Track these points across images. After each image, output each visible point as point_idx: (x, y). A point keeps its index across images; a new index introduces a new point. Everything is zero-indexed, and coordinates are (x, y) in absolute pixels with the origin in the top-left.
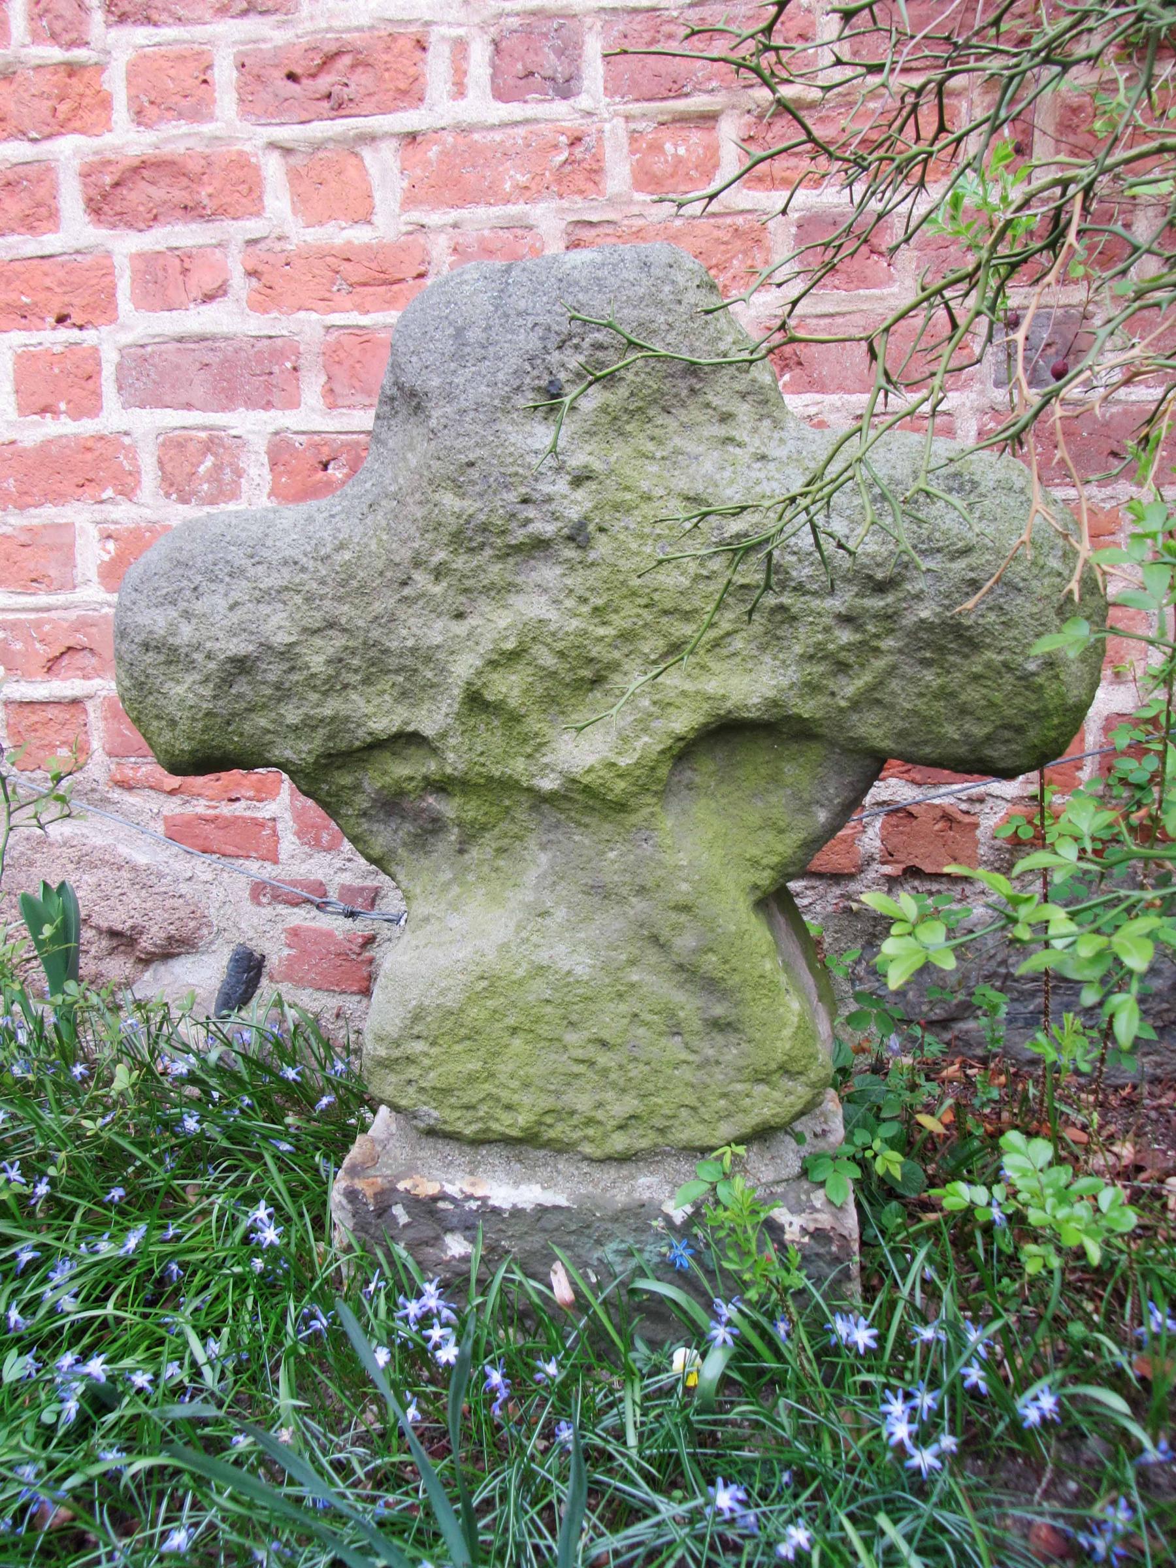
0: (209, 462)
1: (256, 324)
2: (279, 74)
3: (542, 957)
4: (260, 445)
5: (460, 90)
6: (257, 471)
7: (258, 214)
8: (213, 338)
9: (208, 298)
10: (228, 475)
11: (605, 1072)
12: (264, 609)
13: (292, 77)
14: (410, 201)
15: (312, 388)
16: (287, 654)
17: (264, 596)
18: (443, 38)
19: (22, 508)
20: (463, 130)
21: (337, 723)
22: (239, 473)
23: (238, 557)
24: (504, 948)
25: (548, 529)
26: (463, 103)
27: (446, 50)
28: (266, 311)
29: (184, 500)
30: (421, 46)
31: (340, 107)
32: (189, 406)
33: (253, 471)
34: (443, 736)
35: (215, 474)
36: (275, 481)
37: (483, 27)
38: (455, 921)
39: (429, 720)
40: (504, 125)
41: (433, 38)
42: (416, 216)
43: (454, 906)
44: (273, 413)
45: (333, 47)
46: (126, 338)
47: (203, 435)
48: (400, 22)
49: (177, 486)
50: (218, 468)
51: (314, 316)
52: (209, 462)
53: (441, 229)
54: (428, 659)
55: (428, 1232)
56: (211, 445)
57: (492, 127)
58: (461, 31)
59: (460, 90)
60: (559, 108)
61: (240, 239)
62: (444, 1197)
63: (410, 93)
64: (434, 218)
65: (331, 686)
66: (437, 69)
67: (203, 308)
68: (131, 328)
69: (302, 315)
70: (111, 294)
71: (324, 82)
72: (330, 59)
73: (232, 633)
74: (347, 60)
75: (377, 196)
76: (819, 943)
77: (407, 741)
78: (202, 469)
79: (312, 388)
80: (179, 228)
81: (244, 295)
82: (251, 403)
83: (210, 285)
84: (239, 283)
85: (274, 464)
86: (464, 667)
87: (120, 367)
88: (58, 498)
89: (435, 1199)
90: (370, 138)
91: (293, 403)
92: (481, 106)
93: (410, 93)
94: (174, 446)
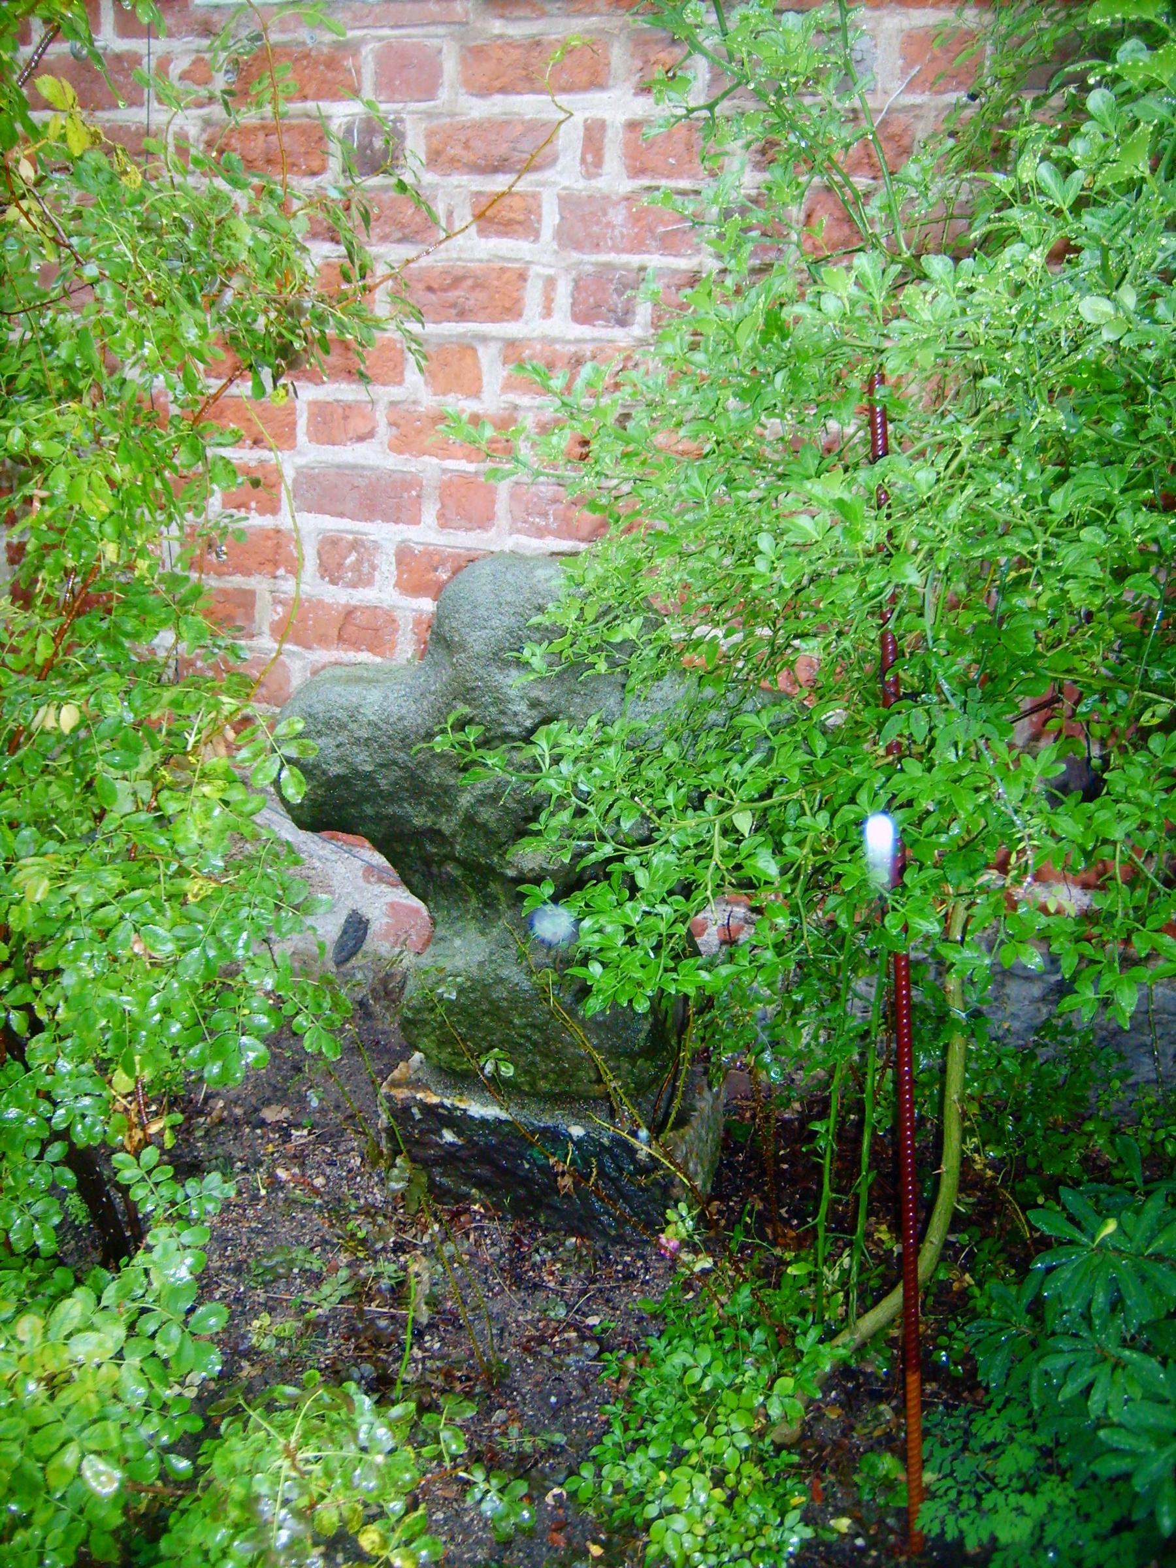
0: (353, 557)
1: (392, 462)
2: (421, 286)
3: (504, 973)
4: (390, 549)
5: (548, 312)
6: (387, 566)
7: (400, 383)
8: (363, 467)
9: (361, 439)
10: (366, 568)
11: (535, 1044)
12: (356, 749)
13: (430, 289)
14: (508, 386)
15: (430, 512)
16: (368, 777)
17: (357, 742)
18: (538, 275)
19: (220, 575)
20: (548, 341)
21: (395, 819)
22: (374, 568)
23: (342, 715)
24: (481, 964)
25: (515, 730)
26: (549, 322)
27: (540, 284)
28: (401, 453)
29: (333, 582)
30: (522, 277)
31: (463, 315)
32: (341, 515)
33: (384, 567)
34: (454, 836)
35: (357, 567)
36: (400, 576)
37: (567, 270)
38: (458, 942)
39: (448, 824)
40: (578, 341)
41: (531, 273)
42: (511, 397)
43: (458, 934)
44: (401, 526)
45: (460, 273)
46: (301, 461)
47: (350, 537)
48: (509, 260)
49: (330, 571)
50: (359, 562)
51: (435, 461)
52: (353, 557)
53: (529, 409)
54: (446, 792)
55: (432, 1124)
56: (355, 545)
57: (569, 342)
58: (551, 272)
59: (548, 312)
60: (617, 333)
61: (386, 399)
62: (442, 1105)
63: (512, 311)
64: (525, 401)
65: (391, 798)
66: (533, 295)
67: (358, 446)
68: (304, 455)
69: (426, 458)
70: (293, 426)
71: (452, 295)
72: (457, 281)
73: (338, 761)
74: (469, 282)
75: (485, 379)
76: (320, 1053)
77: (434, 834)
78: (348, 561)
79: (430, 512)
80: (344, 386)
81: (386, 439)
82: (386, 518)
83: (364, 429)
84: (384, 432)
85: (399, 562)
86: (465, 800)
87: (295, 481)
88: (248, 573)
89: (437, 1106)
90: (484, 339)
91: (415, 520)
92: (562, 327)
93: (512, 311)
94: (330, 545)
